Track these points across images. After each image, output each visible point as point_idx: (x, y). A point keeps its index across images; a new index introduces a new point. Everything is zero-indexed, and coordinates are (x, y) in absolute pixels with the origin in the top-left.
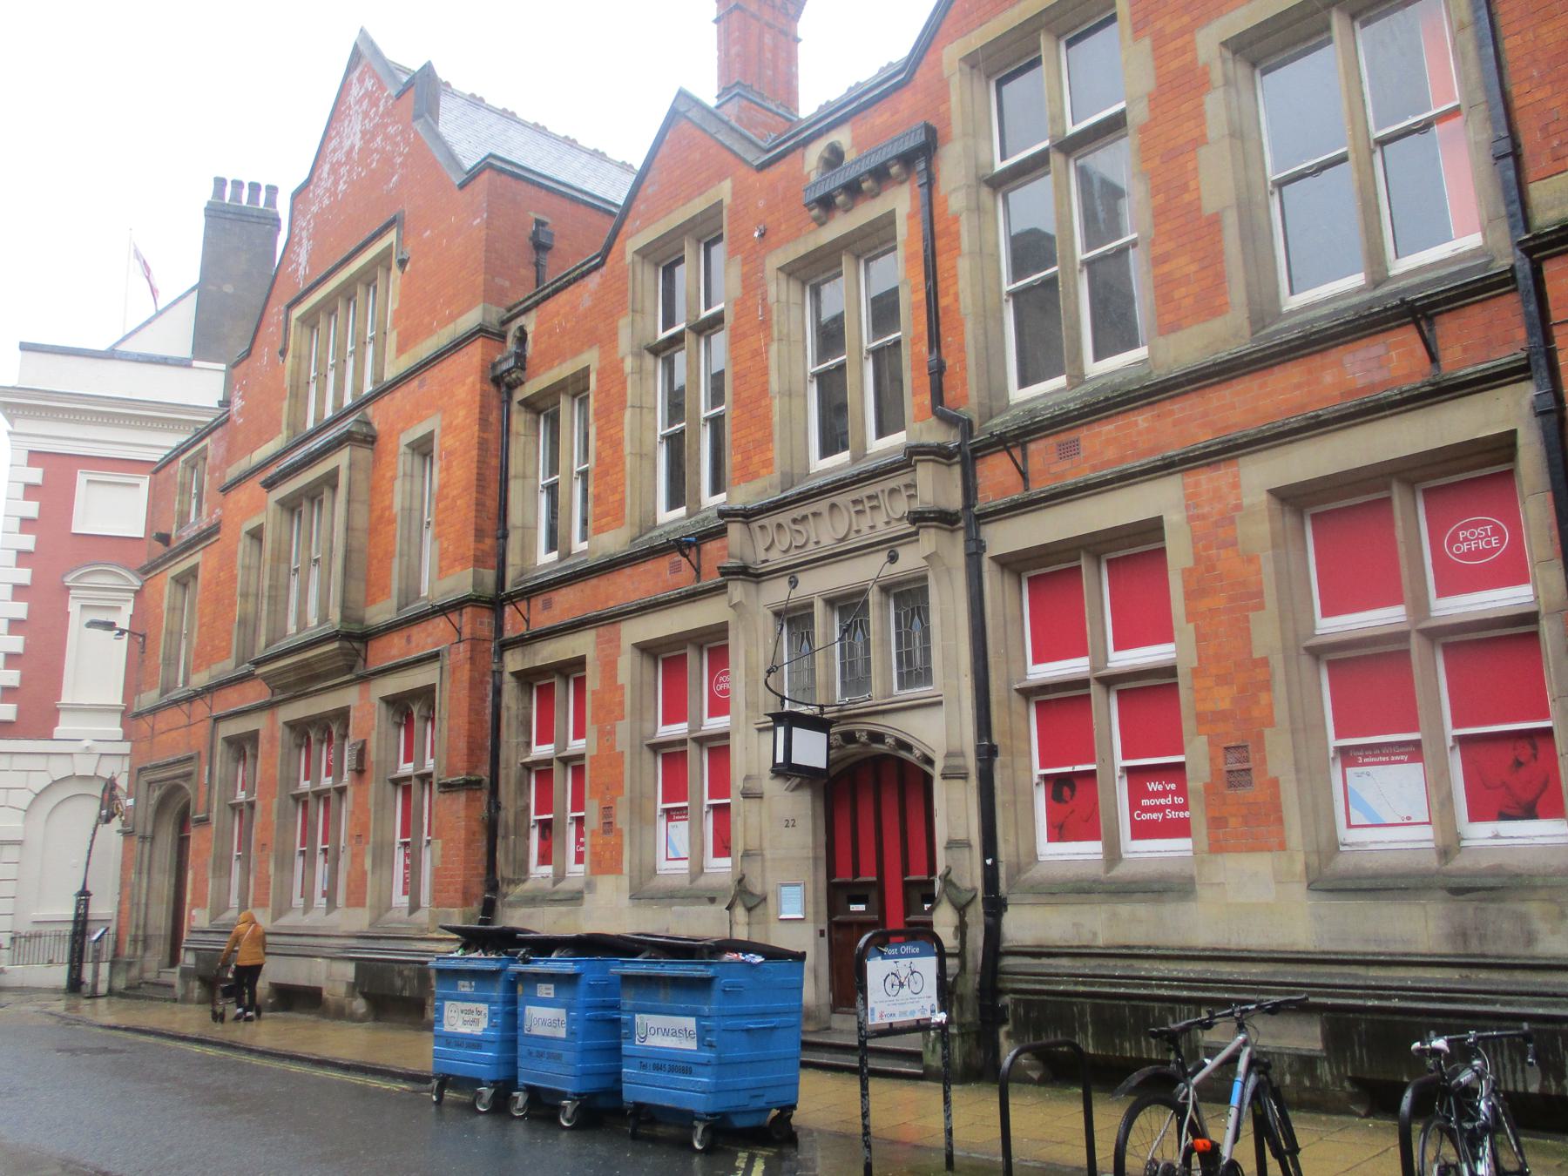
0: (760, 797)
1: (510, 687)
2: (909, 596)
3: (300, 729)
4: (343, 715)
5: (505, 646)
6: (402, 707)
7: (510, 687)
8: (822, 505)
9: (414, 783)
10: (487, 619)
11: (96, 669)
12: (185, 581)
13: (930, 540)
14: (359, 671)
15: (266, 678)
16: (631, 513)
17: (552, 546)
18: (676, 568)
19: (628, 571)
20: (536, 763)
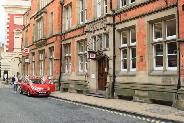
0: (90, 62)
1: (63, 46)
2: (107, 35)
3: (40, 52)
4: (44, 50)
5: (62, 41)
6: (51, 49)
7: (63, 46)
8: (97, 22)
9: (68, 57)
10: (60, 37)
11: (17, 43)
12: (27, 31)
13: (108, 28)
14: (46, 44)
15: (35, 45)
16: (77, 23)
17: (82, 21)
18: (81, 31)
19: (76, 31)
20: (66, 57)
